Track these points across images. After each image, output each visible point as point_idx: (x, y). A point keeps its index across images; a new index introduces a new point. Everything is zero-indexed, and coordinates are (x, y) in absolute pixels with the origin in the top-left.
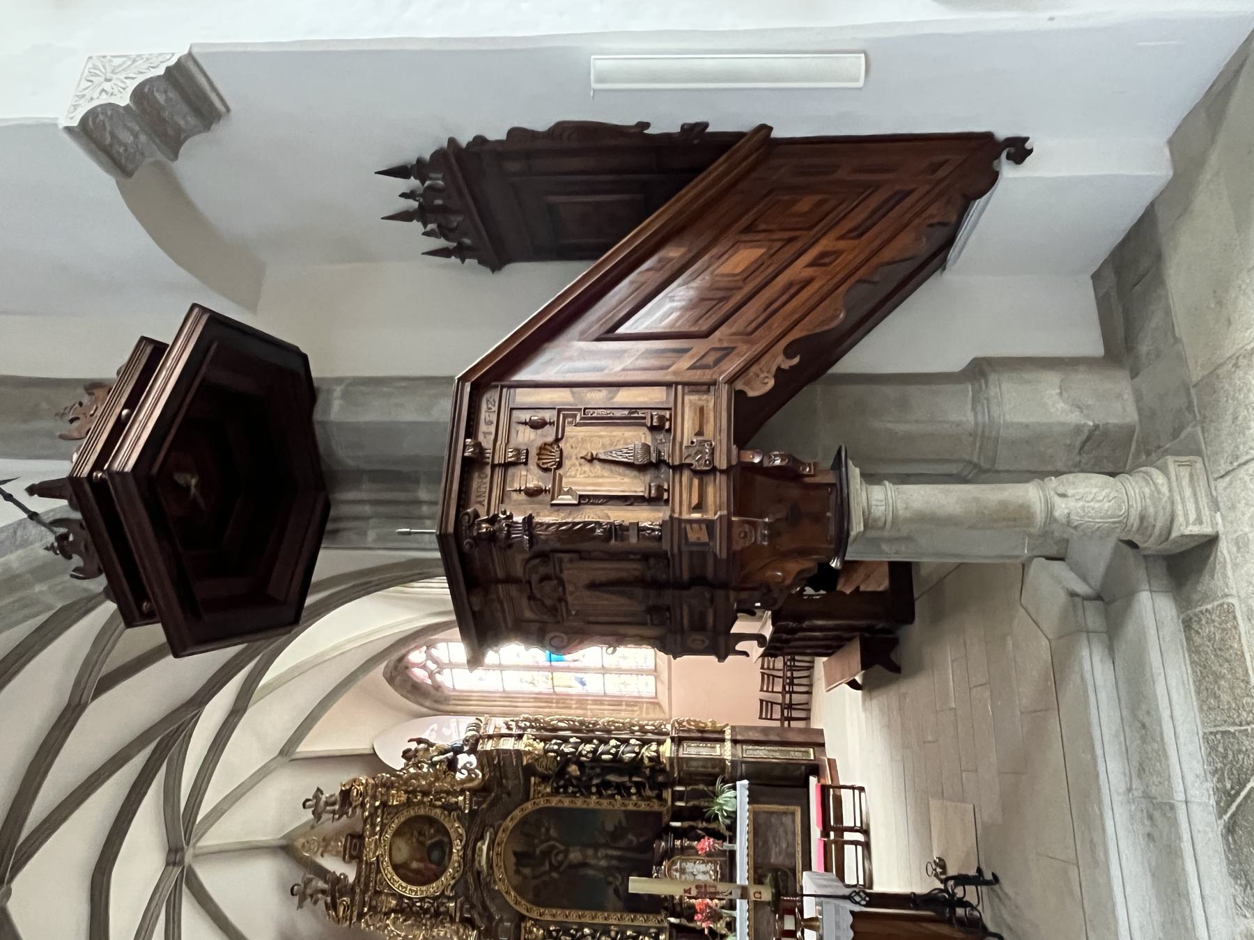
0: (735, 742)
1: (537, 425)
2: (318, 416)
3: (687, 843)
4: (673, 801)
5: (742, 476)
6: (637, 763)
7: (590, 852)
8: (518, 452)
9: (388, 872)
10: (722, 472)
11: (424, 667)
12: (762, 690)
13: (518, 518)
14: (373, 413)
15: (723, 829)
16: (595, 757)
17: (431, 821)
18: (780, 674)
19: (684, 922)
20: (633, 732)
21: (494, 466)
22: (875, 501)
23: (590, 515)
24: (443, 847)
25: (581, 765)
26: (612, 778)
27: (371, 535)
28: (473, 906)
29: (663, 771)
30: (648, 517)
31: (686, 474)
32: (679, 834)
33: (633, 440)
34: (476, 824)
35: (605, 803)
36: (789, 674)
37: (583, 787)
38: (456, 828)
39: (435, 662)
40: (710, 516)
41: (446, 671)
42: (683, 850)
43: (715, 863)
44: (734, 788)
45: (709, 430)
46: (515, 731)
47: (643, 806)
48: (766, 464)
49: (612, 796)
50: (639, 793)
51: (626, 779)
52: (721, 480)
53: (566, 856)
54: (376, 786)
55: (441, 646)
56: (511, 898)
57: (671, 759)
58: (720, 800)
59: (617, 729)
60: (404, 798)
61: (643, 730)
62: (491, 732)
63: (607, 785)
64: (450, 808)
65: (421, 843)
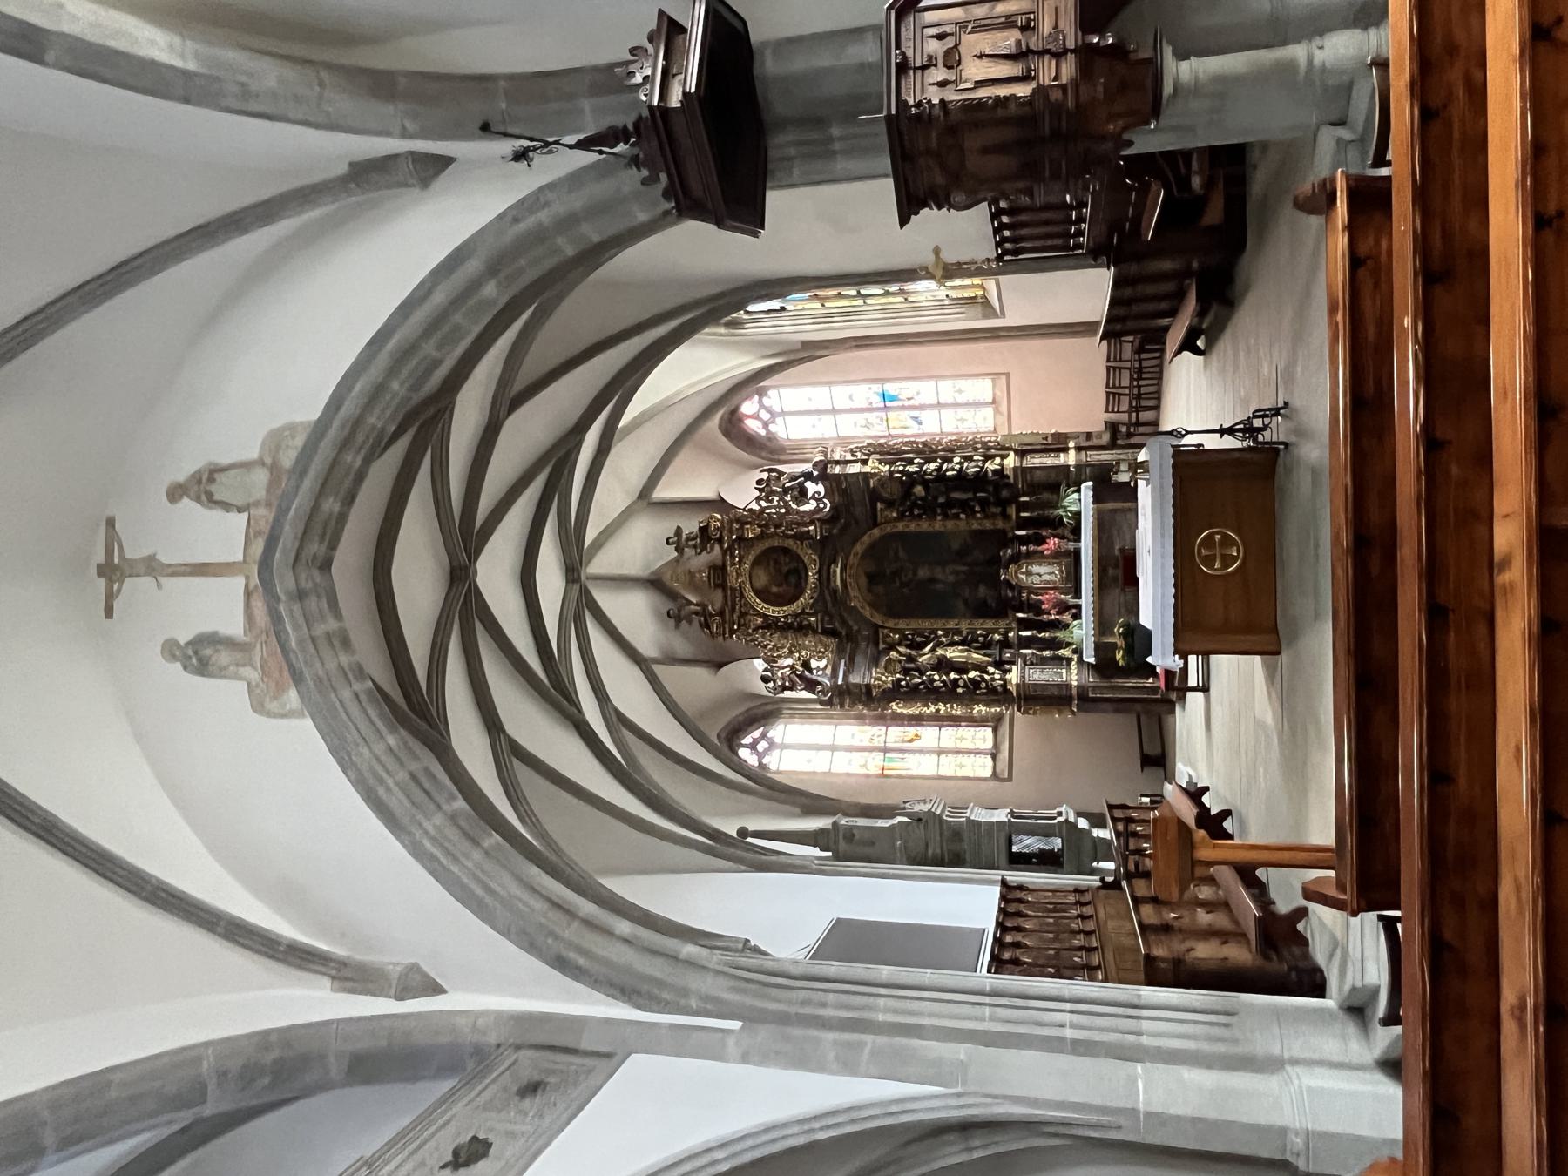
0: (1079, 449)
1: (941, 37)
2: (757, 71)
3: (1032, 548)
4: (1018, 512)
5: (1086, 54)
6: (981, 477)
7: (938, 569)
8: (930, 57)
9: (751, 596)
10: (1072, 51)
11: (756, 417)
12: (1107, 411)
13: (936, 101)
14: (800, 63)
15: (1067, 533)
16: (940, 476)
17: (786, 551)
18: (1128, 365)
19: (1031, 616)
20: (976, 449)
21: (915, 69)
22: (1181, 71)
23: (982, 93)
24: (799, 573)
25: (926, 484)
26: (956, 495)
27: (796, 172)
28: (831, 617)
29: (1008, 485)
30: (1023, 90)
31: (1047, 57)
32: (1024, 541)
33: (1008, 40)
34: (828, 548)
35: (950, 525)
36: (1136, 391)
37: (929, 508)
38: (810, 557)
39: (769, 410)
40: (1064, 80)
41: (779, 420)
42: (1029, 554)
43: (1060, 564)
44: (1079, 491)
45: (1061, 25)
46: (860, 456)
47: (988, 525)
48: (1103, 44)
49: (957, 516)
50: (983, 511)
51: (970, 495)
52: (1071, 57)
53: (915, 574)
54: (731, 522)
55: (772, 393)
56: (867, 612)
57: (1015, 469)
58: (1065, 503)
59: (961, 448)
60: (758, 530)
61: (984, 444)
62: (837, 458)
63: (950, 504)
64: (803, 537)
65: (779, 571)
